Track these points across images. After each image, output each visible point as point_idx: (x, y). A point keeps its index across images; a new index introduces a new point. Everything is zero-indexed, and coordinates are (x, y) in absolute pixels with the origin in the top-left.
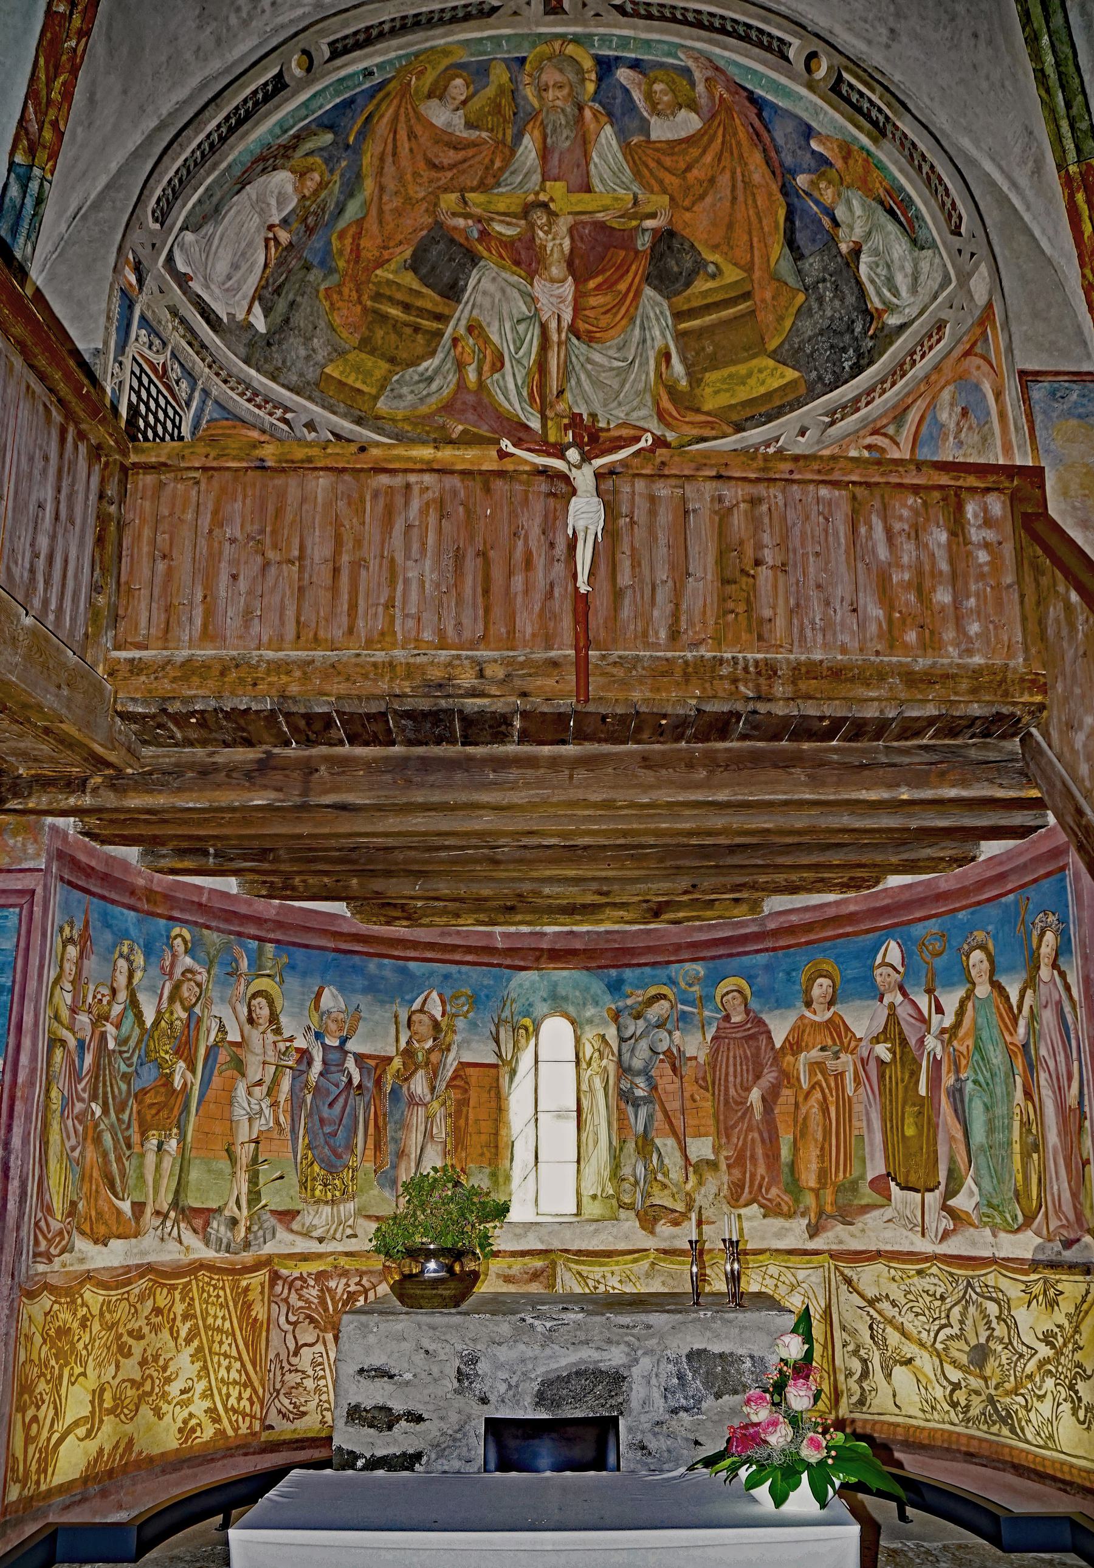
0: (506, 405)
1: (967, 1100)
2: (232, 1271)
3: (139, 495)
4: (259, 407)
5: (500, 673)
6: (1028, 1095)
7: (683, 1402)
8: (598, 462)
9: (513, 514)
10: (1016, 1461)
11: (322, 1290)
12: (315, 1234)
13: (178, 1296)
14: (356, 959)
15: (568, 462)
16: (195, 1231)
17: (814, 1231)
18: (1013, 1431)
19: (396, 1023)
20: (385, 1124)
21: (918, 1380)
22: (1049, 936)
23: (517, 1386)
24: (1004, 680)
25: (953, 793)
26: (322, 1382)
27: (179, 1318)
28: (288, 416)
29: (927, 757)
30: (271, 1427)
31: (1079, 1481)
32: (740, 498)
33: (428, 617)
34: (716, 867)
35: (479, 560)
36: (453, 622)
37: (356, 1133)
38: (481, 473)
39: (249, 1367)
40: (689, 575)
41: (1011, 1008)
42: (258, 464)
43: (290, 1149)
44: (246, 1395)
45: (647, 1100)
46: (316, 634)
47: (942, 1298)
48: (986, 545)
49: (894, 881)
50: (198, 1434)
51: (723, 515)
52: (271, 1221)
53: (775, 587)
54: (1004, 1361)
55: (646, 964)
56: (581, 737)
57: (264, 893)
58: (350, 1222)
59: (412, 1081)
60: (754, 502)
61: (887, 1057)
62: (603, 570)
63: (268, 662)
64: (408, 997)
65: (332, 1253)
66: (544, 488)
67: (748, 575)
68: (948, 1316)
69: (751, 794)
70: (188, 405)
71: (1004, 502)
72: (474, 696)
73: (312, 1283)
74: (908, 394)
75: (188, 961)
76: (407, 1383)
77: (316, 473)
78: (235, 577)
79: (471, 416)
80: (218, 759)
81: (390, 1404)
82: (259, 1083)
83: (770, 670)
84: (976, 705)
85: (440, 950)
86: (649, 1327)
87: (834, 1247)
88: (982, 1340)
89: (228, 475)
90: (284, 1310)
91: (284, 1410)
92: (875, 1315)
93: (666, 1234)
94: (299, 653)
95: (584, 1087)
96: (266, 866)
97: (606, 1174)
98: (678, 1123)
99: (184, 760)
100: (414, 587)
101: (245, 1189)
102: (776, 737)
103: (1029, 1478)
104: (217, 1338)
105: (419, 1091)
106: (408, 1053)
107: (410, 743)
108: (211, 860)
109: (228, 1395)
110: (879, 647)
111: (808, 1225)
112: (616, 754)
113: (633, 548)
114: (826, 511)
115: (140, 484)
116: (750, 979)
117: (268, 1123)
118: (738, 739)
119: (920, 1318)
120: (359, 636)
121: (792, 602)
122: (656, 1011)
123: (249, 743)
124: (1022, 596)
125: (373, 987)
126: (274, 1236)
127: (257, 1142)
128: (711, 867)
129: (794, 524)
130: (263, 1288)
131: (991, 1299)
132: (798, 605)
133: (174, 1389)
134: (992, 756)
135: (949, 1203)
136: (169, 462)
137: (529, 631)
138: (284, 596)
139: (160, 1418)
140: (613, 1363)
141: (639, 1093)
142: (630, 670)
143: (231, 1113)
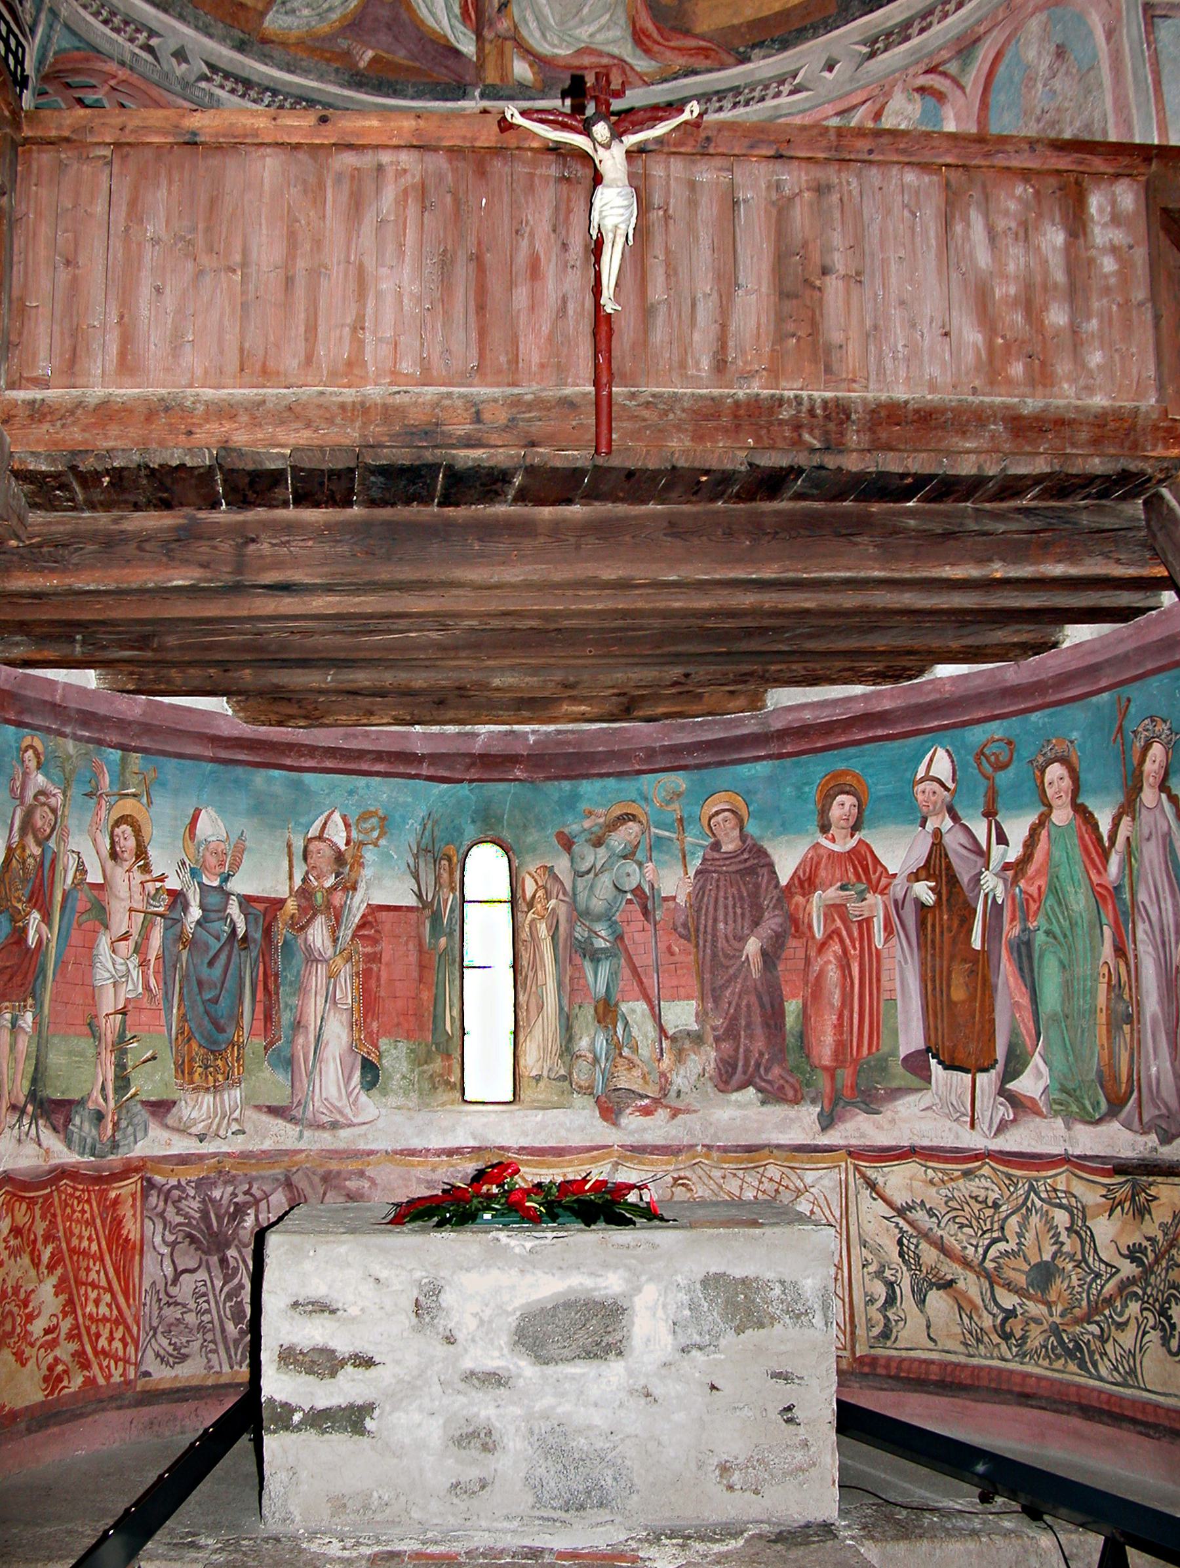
0: (431, 22)
1: (1036, 955)
2: (98, 1179)
3: (34, 180)
4: (117, 30)
5: (503, 417)
6: (1120, 951)
7: (697, 1338)
8: (631, 140)
9: (514, 205)
10: (1084, 1402)
11: (203, 1201)
12: (194, 1130)
13: (38, 1213)
14: (240, 771)
15: (594, 140)
16: (55, 1129)
17: (827, 1122)
18: (1082, 1365)
19: (290, 855)
20: (277, 987)
21: (960, 1308)
22: (1157, 750)
23: (490, 1322)
24: (1133, 427)
25: (1058, 570)
26: (206, 1318)
27: (40, 1240)
28: (154, 42)
29: (1025, 523)
30: (147, 1374)
31: (1166, 1423)
32: (804, 185)
33: (409, 341)
34: (728, 654)
35: (473, 266)
36: (439, 349)
37: (241, 1002)
38: (473, 149)
39: (121, 1299)
40: (737, 285)
41: (1099, 838)
42: (187, 138)
43: (163, 1022)
44: (118, 1335)
45: (608, 953)
46: (264, 365)
47: (996, 1205)
48: (1114, 250)
49: (944, 671)
50: (65, 1383)
51: (781, 209)
52: (144, 1114)
53: (848, 303)
54: (1075, 1282)
55: (608, 775)
56: (591, 496)
57: (131, 687)
58: (236, 1114)
59: (310, 931)
60: (821, 189)
61: (929, 898)
62: (629, 283)
63: (207, 404)
64: (303, 820)
65: (215, 1155)
66: (554, 171)
67: (814, 287)
68: (1002, 1228)
69: (805, 570)
70: (33, 31)
71: (1137, 194)
72: (469, 446)
73: (192, 1193)
74: (980, 22)
75: (41, 779)
76: (354, 1319)
77: (262, 150)
78: (159, 291)
79: (385, 38)
80: (127, 526)
81: (332, 1345)
82: (125, 937)
83: (838, 413)
84: (1097, 460)
85: (342, 757)
86: (654, 1246)
87: (853, 1142)
88: (1047, 1257)
89: (149, 153)
90: (160, 1227)
91: (162, 1352)
92: (906, 1227)
93: (632, 1127)
94: (246, 391)
95: (525, 934)
96: (149, 655)
97: (556, 1047)
98: (651, 982)
99: (82, 528)
100: (389, 300)
101: (111, 1075)
102: (841, 497)
103: (1100, 1422)
104: (84, 1264)
105: (319, 944)
106: (305, 893)
107: (372, 503)
108: (78, 649)
109: (98, 1335)
110: (977, 383)
111: (820, 1115)
112: (636, 517)
113: (667, 251)
114: (913, 204)
115: (35, 166)
116: (747, 795)
117: (136, 989)
118: (790, 499)
119: (966, 1230)
120: (319, 367)
121: (868, 323)
122: (619, 839)
123: (166, 505)
124: (1157, 318)
125: (260, 809)
126: (146, 1134)
127: (123, 1012)
128: (720, 654)
129: (872, 219)
130: (134, 1200)
131: (1061, 1206)
132: (876, 328)
133: (37, 1327)
134: (1108, 522)
135: (1008, 1086)
136: (74, 137)
137: (535, 359)
138: (222, 315)
139: (23, 1365)
140: (609, 1292)
141: (600, 944)
142: (666, 413)
143: (92, 976)
